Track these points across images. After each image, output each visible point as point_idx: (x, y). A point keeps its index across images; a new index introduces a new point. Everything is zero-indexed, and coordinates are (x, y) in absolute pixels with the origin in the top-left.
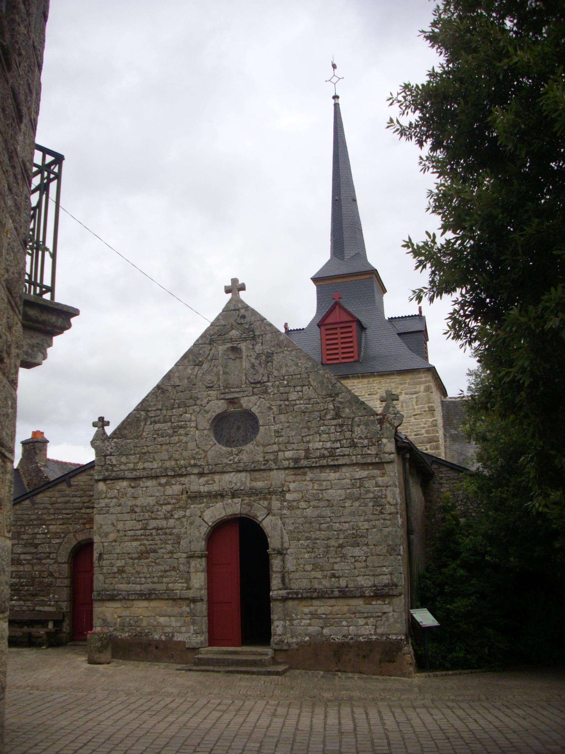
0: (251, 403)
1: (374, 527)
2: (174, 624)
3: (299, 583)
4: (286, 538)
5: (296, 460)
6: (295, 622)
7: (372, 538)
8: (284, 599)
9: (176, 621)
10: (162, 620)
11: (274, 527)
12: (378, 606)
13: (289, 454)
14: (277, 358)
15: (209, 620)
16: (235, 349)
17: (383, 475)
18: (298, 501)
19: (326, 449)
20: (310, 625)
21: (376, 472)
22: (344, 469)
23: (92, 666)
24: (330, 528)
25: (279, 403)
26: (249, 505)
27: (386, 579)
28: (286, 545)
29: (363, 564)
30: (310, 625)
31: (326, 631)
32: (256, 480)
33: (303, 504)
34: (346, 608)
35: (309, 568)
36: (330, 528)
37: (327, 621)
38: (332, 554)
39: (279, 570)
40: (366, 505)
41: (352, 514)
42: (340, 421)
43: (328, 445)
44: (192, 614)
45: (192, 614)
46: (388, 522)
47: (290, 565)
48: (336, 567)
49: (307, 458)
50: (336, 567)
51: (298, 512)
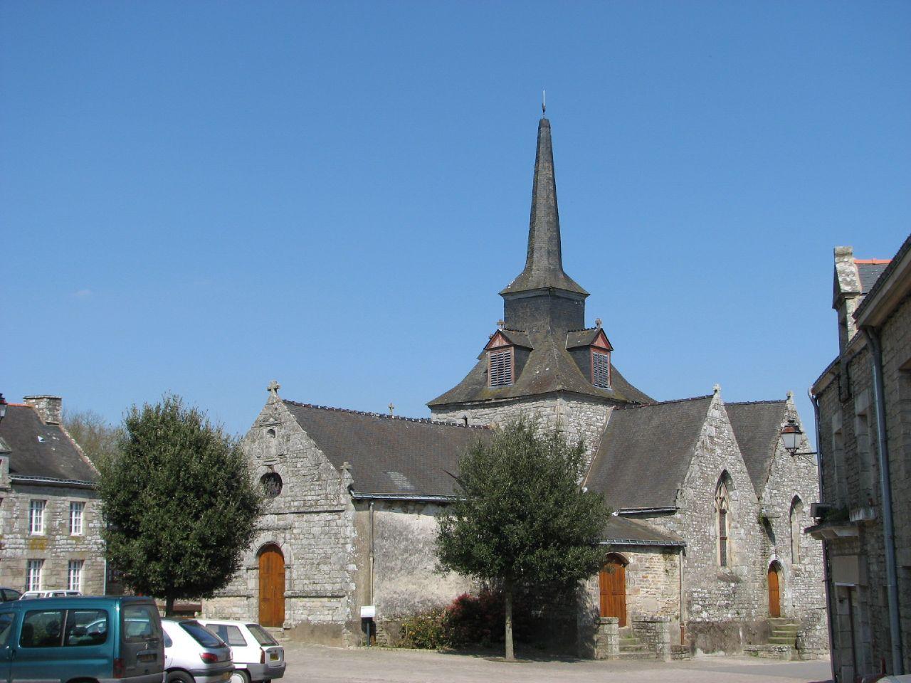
0: (279, 469)
1: (334, 552)
2: (240, 612)
3: (298, 588)
4: (293, 558)
5: (298, 507)
6: (296, 612)
7: (333, 559)
8: (291, 597)
9: (242, 610)
10: (235, 609)
11: (287, 549)
12: (334, 602)
13: (296, 503)
14: (292, 438)
15: (822, 465)
16: (272, 432)
17: (340, 518)
18: (299, 534)
19: (314, 501)
20: (302, 614)
21: (337, 517)
22: (321, 514)
23: (90, 676)
24: (313, 553)
25: (292, 469)
26: (276, 536)
27: (338, 586)
28: (293, 563)
29: (328, 576)
30: (302, 614)
31: (310, 618)
32: (279, 520)
33: (301, 537)
34: (319, 604)
35: (303, 577)
36: (313, 553)
37: (311, 611)
38: (314, 569)
39: (669, 641)
40: (330, 538)
41: (324, 543)
42: (320, 482)
43: (315, 498)
44: (248, 606)
45: (248, 606)
46: (340, 550)
47: (294, 576)
48: (316, 577)
49: (304, 506)
50: (316, 577)
51: (299, 541)
